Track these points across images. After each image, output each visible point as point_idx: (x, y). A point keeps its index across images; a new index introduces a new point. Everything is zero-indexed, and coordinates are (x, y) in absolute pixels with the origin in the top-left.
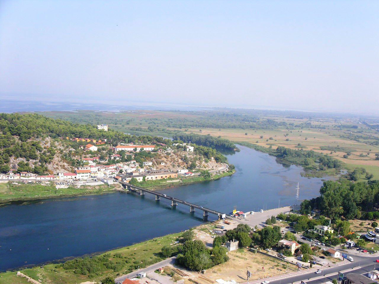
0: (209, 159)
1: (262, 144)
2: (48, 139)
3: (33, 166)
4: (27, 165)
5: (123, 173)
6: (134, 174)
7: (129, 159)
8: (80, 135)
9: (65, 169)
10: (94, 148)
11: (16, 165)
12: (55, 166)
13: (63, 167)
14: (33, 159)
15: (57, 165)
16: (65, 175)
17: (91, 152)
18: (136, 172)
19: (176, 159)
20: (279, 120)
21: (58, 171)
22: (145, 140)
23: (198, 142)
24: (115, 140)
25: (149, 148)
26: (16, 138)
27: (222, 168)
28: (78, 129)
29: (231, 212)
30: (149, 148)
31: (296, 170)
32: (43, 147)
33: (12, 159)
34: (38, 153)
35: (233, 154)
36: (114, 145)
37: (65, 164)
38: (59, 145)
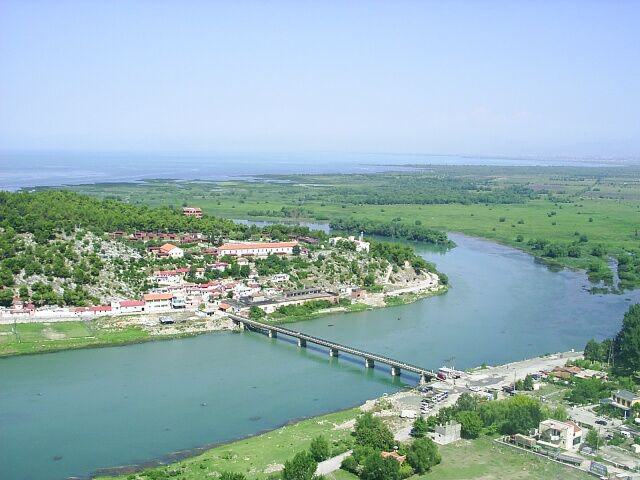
0: (400, 265)
1: (502, 230)
2: (89, 236)
3: (62, 290)
4: (50, 289)
5: (234, 297)
6: (255, 300)
7: (245, 273)
8: (153, 228)
9: (123, 294)
10: (177, 253)
11: (29, 288)
12: (104, 289)
13: (119, 291)
14: (61, 277)
15: (107, 286)
16: (123, 305)
17: (171, 260)
18: (258, 295)
19: (336, 268)
20: (535, 182)
21: (109, 298)
22: (278, 234)
23: (382, 233)
24: (216, 235)
25: (286, 249)
26: (28, 239)
27: (428, 282)
28: (144, 218)
29: (347, 474)
30: (286, 249)
31: (574, 279)
32: (78, 252)
33: (19, 278)
34: (68, 264)
35: (439, 254)
36: (215, 245)
37: (123, 284)
38: (112, 250)
